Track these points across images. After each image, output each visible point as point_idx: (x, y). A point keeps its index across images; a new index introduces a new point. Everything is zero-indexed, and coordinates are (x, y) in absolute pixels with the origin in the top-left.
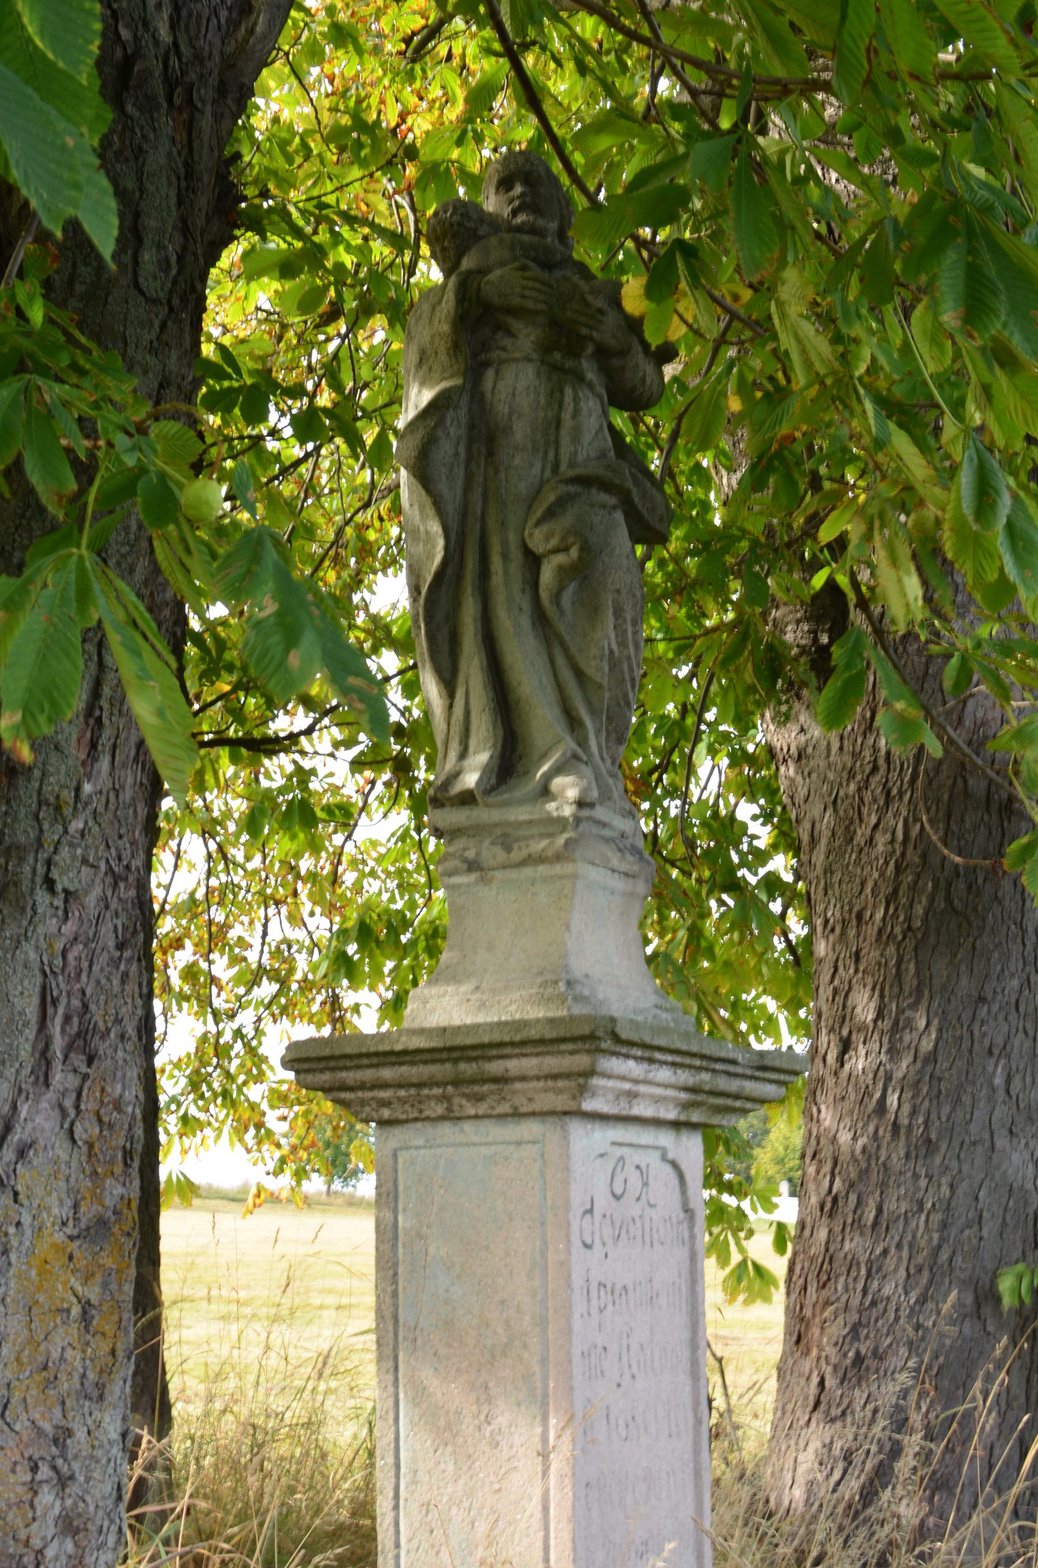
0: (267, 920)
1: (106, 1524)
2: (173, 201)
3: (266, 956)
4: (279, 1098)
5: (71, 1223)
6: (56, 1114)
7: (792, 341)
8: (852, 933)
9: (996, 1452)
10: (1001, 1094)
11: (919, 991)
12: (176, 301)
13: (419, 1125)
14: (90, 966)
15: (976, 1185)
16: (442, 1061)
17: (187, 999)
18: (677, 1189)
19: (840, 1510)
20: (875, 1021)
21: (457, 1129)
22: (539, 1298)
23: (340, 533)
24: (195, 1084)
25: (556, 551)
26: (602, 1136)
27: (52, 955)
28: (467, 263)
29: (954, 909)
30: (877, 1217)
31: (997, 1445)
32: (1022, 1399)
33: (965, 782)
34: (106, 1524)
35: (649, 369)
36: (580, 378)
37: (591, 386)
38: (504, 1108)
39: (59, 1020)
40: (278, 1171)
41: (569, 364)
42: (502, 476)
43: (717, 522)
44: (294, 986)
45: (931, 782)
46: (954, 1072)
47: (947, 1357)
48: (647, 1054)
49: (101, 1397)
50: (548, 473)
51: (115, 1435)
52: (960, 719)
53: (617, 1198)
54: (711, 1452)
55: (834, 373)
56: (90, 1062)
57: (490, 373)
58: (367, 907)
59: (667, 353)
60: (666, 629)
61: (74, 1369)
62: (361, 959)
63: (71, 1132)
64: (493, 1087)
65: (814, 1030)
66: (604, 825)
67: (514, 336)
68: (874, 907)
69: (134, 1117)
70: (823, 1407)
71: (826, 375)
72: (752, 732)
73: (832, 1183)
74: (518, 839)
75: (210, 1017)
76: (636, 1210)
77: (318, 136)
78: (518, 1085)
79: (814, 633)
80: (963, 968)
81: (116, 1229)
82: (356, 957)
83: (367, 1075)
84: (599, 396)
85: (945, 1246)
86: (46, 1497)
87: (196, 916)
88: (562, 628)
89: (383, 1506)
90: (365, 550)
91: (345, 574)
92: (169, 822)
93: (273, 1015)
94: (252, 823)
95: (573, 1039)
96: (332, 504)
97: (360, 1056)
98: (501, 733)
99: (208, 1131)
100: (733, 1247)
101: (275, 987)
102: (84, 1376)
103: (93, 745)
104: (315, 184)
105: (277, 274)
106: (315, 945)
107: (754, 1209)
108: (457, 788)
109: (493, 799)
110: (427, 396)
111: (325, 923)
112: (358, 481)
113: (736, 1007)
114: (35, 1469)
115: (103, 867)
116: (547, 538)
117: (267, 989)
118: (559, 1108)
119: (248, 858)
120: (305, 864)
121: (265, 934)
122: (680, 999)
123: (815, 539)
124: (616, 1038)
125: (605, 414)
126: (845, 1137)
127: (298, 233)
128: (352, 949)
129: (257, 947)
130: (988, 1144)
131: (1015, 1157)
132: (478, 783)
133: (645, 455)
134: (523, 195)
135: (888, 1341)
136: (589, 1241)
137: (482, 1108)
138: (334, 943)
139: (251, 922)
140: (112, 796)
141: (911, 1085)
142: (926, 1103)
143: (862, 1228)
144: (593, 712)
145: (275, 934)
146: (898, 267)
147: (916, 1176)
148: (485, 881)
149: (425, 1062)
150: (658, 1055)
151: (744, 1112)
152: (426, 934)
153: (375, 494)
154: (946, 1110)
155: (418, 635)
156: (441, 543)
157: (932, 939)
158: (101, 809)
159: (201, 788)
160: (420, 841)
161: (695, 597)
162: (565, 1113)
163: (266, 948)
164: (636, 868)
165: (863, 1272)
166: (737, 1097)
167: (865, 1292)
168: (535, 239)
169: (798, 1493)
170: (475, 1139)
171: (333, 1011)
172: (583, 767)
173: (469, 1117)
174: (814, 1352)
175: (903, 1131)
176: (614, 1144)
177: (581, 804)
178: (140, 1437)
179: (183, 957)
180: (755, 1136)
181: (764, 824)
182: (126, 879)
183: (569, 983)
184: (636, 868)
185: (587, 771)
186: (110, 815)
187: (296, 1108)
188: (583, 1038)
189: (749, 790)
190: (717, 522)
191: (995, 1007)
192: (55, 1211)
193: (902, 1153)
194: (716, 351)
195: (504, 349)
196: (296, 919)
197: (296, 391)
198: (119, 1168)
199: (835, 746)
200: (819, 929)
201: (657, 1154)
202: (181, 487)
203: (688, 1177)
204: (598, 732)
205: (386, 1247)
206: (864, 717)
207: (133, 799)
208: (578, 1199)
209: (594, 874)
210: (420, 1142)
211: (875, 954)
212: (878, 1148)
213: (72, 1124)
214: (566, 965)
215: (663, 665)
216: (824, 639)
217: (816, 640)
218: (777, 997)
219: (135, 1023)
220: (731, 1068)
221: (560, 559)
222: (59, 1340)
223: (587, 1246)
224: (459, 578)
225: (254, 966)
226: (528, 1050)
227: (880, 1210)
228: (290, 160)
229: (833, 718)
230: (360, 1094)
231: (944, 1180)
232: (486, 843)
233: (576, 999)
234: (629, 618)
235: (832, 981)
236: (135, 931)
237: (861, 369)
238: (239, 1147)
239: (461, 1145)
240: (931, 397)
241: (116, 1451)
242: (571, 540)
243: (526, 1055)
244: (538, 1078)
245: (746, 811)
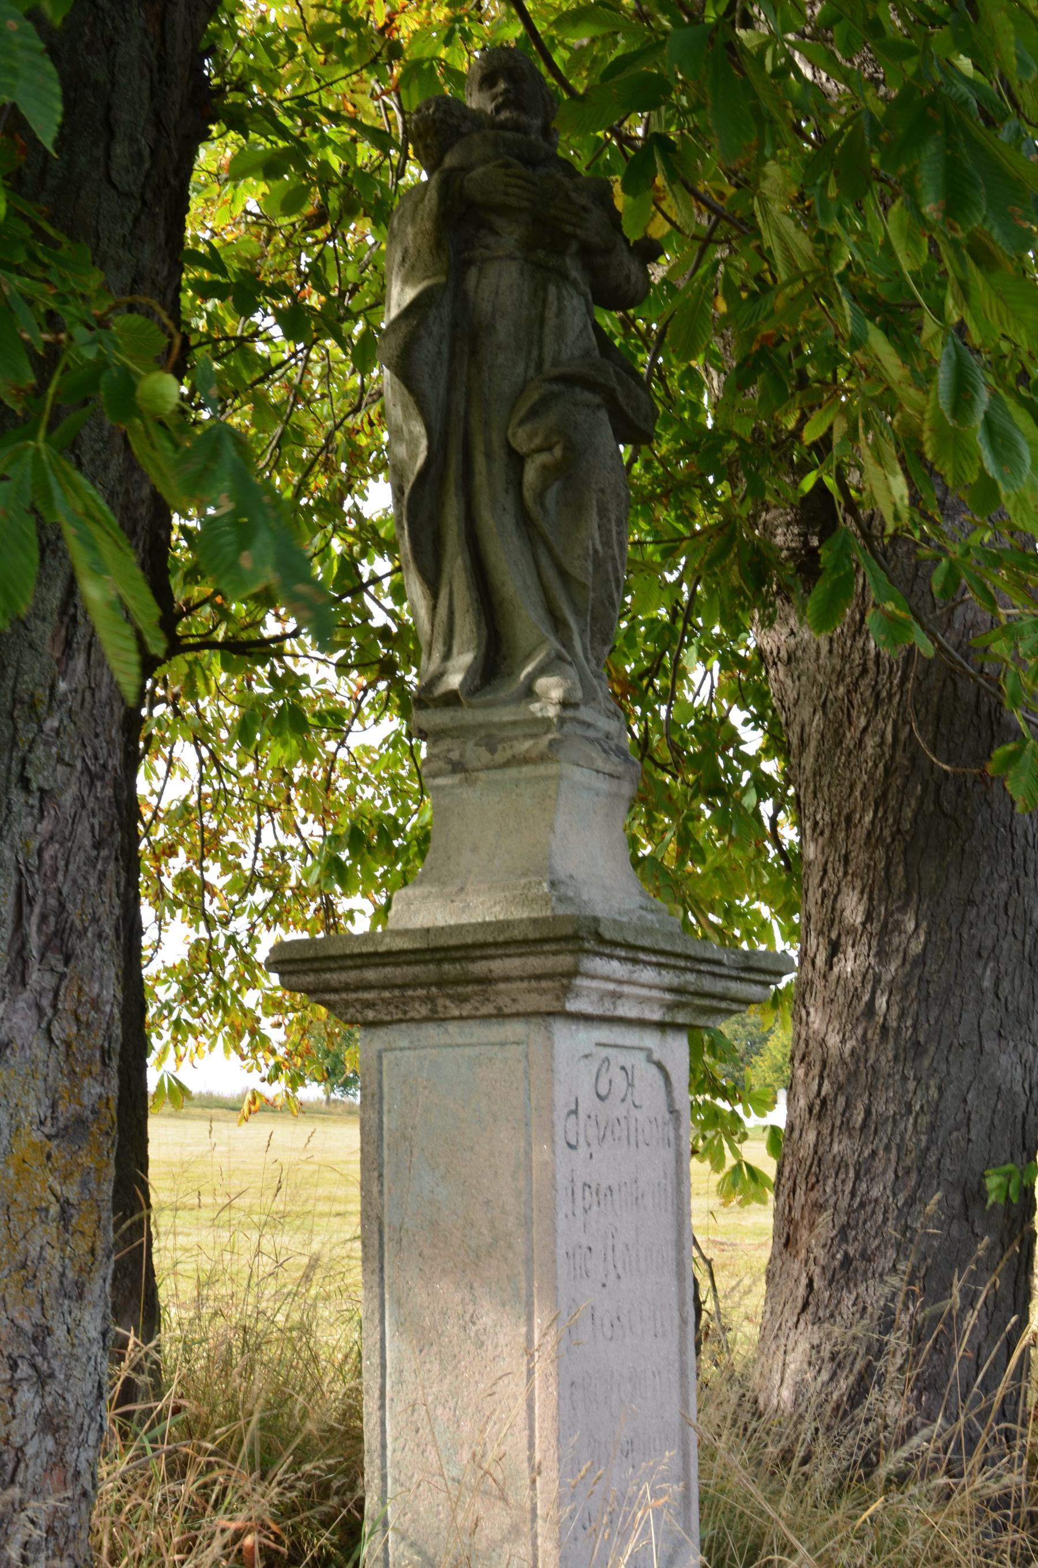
0: (260, 826)
1: (87, 1421)
2: (146, 94)
3: (259, 864)
4: (274, 1005)
5: (49, 1122)
6: (33, 1013)
7: (774, 237)
8: (841, 835)
9: (984, 1352)
10: (990, 996)
11: (908, 893)
12: (149, 196)
13: (404, 1026)
14: (67, 865)
15: (964, 1088)
16: (425, 962)
17: (180, 905)
18: (663, 1090)
19: (829, 1408)
20: (864, 924)
21: (442, 1030)
22: (523, 1198)
23: (330, 437)
24: (188, 991)
25: (539, 450)
26: (587, 1037)
27: (28, 855)
28: (450, 160)
29: (943, 812)
30: (865, 1120)
31: (984, 1345)
32: (1010, 1301)
33: (955, 684)
34: (87, 1421)
35: (634, 268)
36: (564, 276)
37: (575, 284)
38: (488, 1009)
39: (34, 920)
40: (271, 1079)
41: (552, 262)
43: (710, 423)
44: (288, 893)
45: (920, 684)
46: (942, 975)
47: (934, 1258)
48: (630, 955)
49: (81, 1296)
50: (531, 371)
51: (94, 1334)
52: (950, 623)
54: (698, 1352)
55: (815, 271)
56: (67, 961)
57: (473, 272)
58: (360, 813)
59: (650, 251)
60: (655, 532)
61: (53, 1267)
62: (353, 865)
63: (48, 1031)
64: (477, 988)
65: (803, 933)
66: (589, 725)
67: (497, 233)
68: (863, 810)
69: (112, 1015)
70: (811, 1308)
71: (807, 273)
72: (743, 635)
73: (820, 1085)
74: (502, 740)
75: (202, 924)
76: (621, 1111)
77: (303, 35)
78: (502, 986)
79: (804, 535)
80: (952, 870)
81: (94, 1129)
82: (348, 863)
83: (351, 976)
84: (583, 295)
85: (933, 1148)
86: (26, 1395)
87: (188, 822)
88: (546, 527)
89: (370, 1406)
90: (356, 456)
91: (336, 478)
92: (160, 729)
93: (267, 922)
94: (244, 731)
95: (557, 940)
96: (322, 409)
97: (345, 957)
98: (485, 633)
99: (202, 1039)
100: (727, 1152)
101: (269, 894)
102: (63, 1275)
103: (68, 643)
104: (301, 84)
105: (261, 174)
106: (309, 851)
107: (747, 1114)
108: (440, 689)
109: (476, 700)
110: (410, 294)
111: (318, 830)
112: (349, 386)
113: (730, 913)
114: (14, 1367)
115: (79, 766)
116: (531, 437)
117: (261, 896)
118: (543, 1009)
119: (241, 765)
120: (298, 772)
121: (258, 840)
122: (666, 902)
123: (801, 443)
124: (600, 939)
125: (590, 313)
126: (833, 1040)
127: (283, 132)
128: (344, 855)
129: (250, 855)
130: (976, 1047)
131: (1004, 1059)
132: (462, 684)
133: (635, 357)
134: (506, 91)
135: (877, 1242)
136: (573, 1142)
137: (466, 1010)
138: (326, 849)
139: (245, 829)
140: (88, 694)
141: (899, 988)
142: (915, 1006)
143: (850, 1130)
144: (578, 612)
145: (268, 840)
146: (875, 161)
147: (905, 1079)
148: (469, 782)
149: (409, 963)
150: (642, 956)
151: (730, 1012)
152: (417, 839)
153: (366, 397)
154: (934, 1012)
155: (401, 536)
156: (424, 443)
157: (921, 842)
158: (76, 707)
159: (193, 695)
160: (412, 747)
161: (682, 498)
162: (550, 1014)
163: (259, 855)
164: (620, 769)
165: (852, 1174)
166: (722, 998)
167: (853, 1194)
168: (519, 136)
169: (786, 1393)
170: (460, 1040)
171: (327, 917)
172: (567, 667)
173: (454, 1018)
174: (803, 1254)
175: (891, 1033)
176: (598, 1044)
177: (565, 704)
178: (127, 1339)
179: (178, 863)
180: (753, 1043)
181: (754, 729)
182: (102, 778)
183: (553, 884)
184: (620, 769)
185: (572, 672)
186: (86, 714)
187: (291, 1016)
188: (565, 939)
189: (740, 697)
190: (710, 423)
191: (984, 910)
192: (33, 1110)
193: (891, 1056)
194: (702, 251)
195: (487, 247)
196: (291, 827)
197: (278, 290)
198: (96, 1068)
199: (825, 648)
200: (808, 832)
201: (642, 1055)
202: (139, 376)
203: (674, 1078)
204: (582, 632)
205: (371, 1149)
206: (853, 619)
207: (110, 698)
208: (562, 1099)
209: (580, 775)
210: (405, 1043)
211: (864, 857)
212: (867, 1050)
213: (49, 1023)
214: (551, 867)
215: (653, 569)
216: (815, 542)
217: (806, 543)
218: (770, 903)
219: (113, 922)
220: (716, 969)
221: (543, 458)
222: (37, 1239)
224: (442, 478)
225: (248, 873)
226: (512, 950)
227: (868, 1112)
228: (274, 59)
229: (823, 621)
230: (344, 996)
231: (932, 1083)
232: (471, 744)
233: (560, 899)
234: (613, 518)
235: (821, 884)
236: (112, 829)
237: (841, 267)
238: (234, 1056)
240: (914, 297)
241: (96, 1349)
242: (555, 439)
243: (509, 956)
244: (522, 979)
245: (737, 716)
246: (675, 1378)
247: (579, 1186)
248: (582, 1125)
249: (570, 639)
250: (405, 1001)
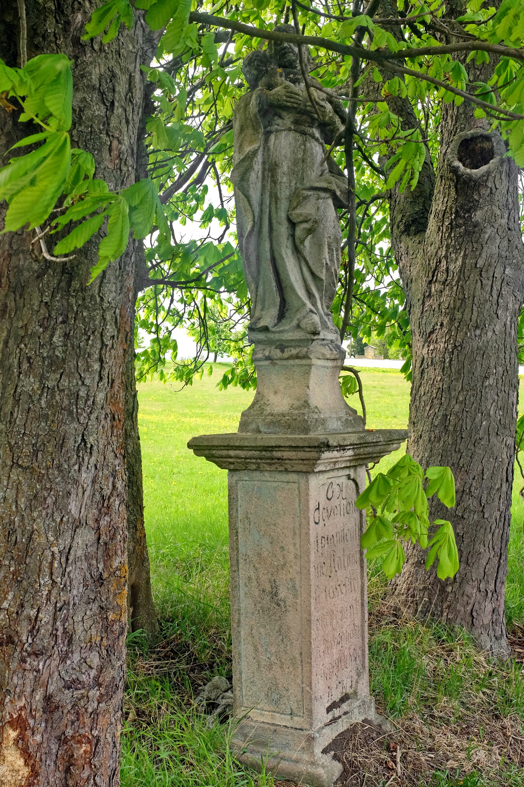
21: (262, 474)
26: (323, 478)
38: (282, 469)
42: (278, 186)
53: (329, 499)
57: (272, 137)
67: (283, 119)
78: (287, 461)
83: (224, 453)
137: (273, 468)
144: (319, 290)
188: (315, 447)
204: (321, 298)
223: (316, 523)
239: (264, 481)
246: (359, 607)
247: (319, 538)
248: (321, 513)
249: (316, 302)
250: (247, 463)
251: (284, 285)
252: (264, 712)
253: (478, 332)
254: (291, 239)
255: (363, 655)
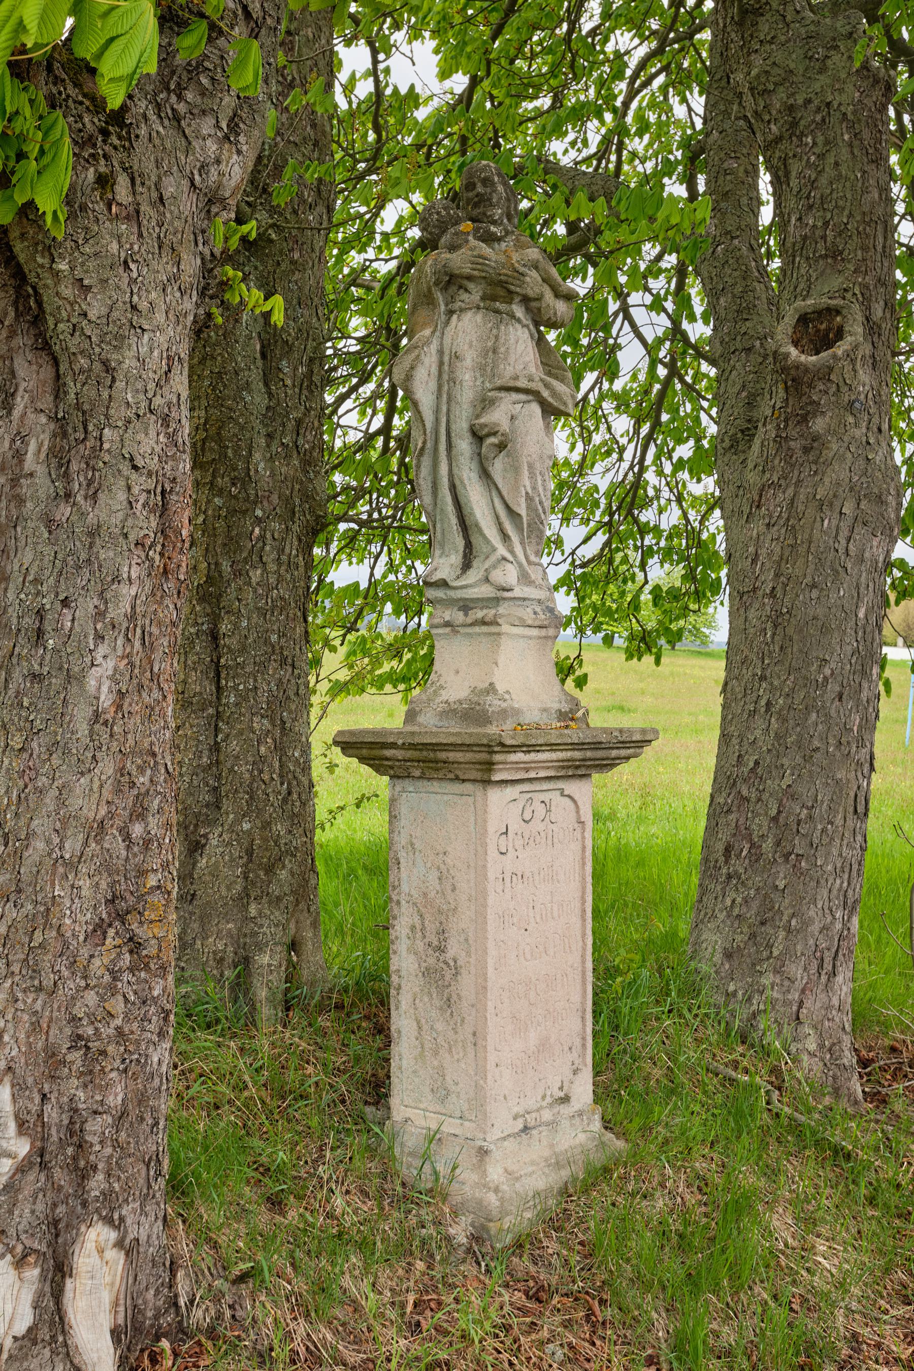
26: (511, 792)
37: (519, 321)
38: (451, 776)
57: (455, 317)
124: (502, 745)
144: (519, 528)
201: (558, 793)
251: (467, 523)
252: (427, 1114)
253: (815, 593)
254: (476, 457)
255: (584, 1046)
